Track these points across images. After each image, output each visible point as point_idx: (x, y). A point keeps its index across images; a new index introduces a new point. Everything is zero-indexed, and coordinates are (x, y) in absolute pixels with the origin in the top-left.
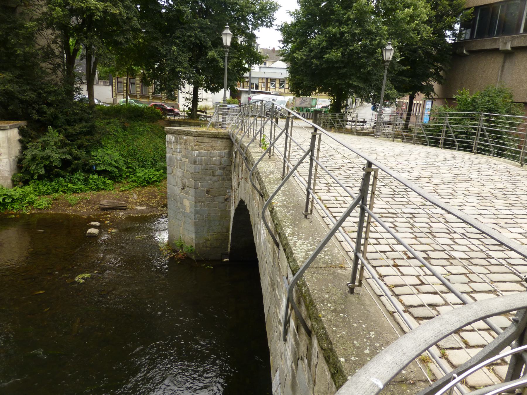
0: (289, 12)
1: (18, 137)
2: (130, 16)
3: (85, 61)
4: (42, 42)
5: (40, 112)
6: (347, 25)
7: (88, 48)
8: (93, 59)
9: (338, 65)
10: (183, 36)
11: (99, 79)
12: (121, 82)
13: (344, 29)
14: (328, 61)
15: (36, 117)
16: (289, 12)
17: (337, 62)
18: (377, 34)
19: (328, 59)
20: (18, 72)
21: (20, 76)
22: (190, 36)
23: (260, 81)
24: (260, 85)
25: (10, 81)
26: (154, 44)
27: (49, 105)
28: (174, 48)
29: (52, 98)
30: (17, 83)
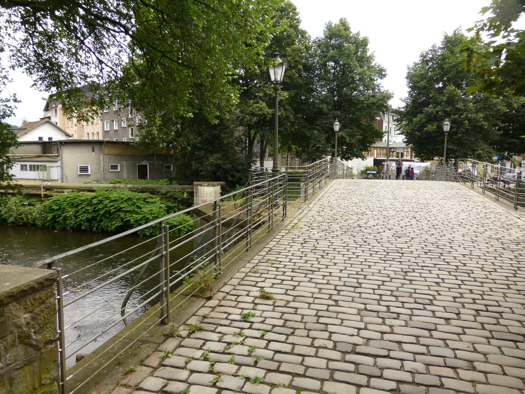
0: (401, 99)
1: (220, 191)
2: (288, 114)
3: (259, 144)
4: (237, 134)
5: (233, 176)
6: (441, 106)
7: (262, 136)
8: (265, 143)
9: (435, 135)
10: (322, 123)
11: (269, 156)
12: (284, 158)
13: (439, 108)
14: (428, 133)
15: (230, 179)
16: (401, 99)
17: (434, 132)
18: (466, 110)
19: (427, 130)
20: (223, 153)
21: (224, 156)
22: (327, 123)
23: (406, 150)
24: (405, 154)
25: (219, 159)
26: (303, 130)
27: (238, 172)
28: (315, 132)
29: (240, 167)
30: (222, 159)
